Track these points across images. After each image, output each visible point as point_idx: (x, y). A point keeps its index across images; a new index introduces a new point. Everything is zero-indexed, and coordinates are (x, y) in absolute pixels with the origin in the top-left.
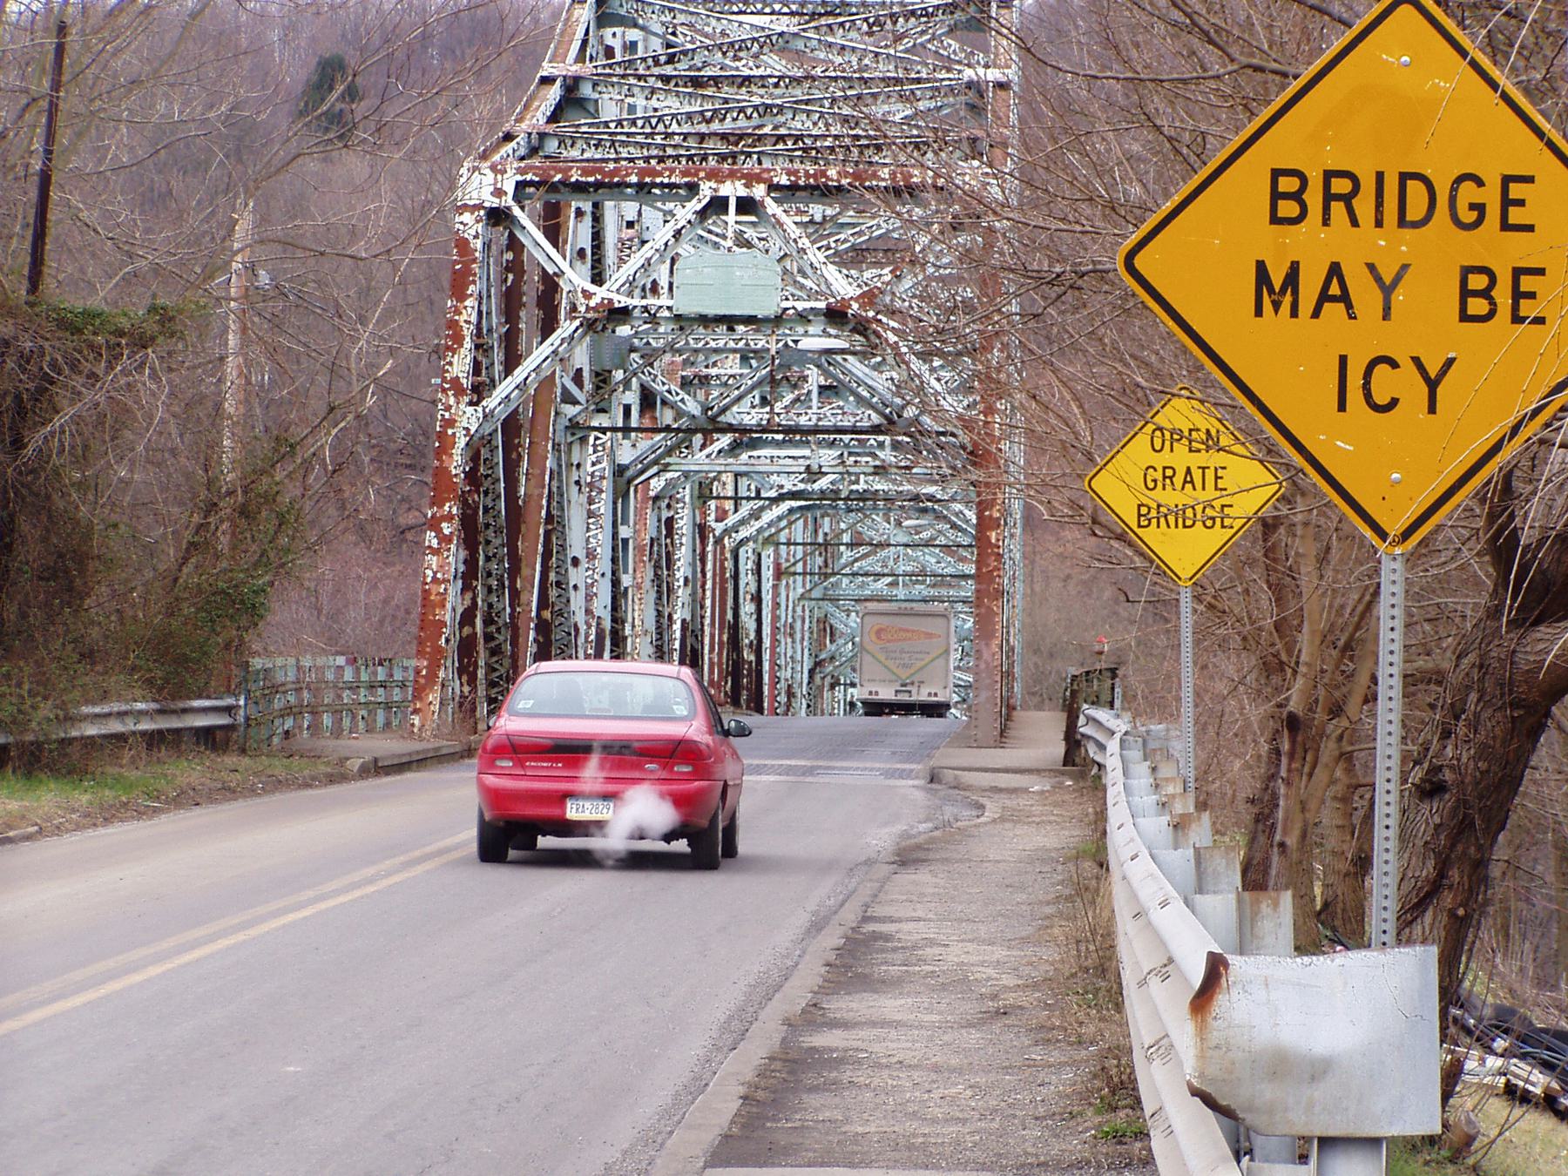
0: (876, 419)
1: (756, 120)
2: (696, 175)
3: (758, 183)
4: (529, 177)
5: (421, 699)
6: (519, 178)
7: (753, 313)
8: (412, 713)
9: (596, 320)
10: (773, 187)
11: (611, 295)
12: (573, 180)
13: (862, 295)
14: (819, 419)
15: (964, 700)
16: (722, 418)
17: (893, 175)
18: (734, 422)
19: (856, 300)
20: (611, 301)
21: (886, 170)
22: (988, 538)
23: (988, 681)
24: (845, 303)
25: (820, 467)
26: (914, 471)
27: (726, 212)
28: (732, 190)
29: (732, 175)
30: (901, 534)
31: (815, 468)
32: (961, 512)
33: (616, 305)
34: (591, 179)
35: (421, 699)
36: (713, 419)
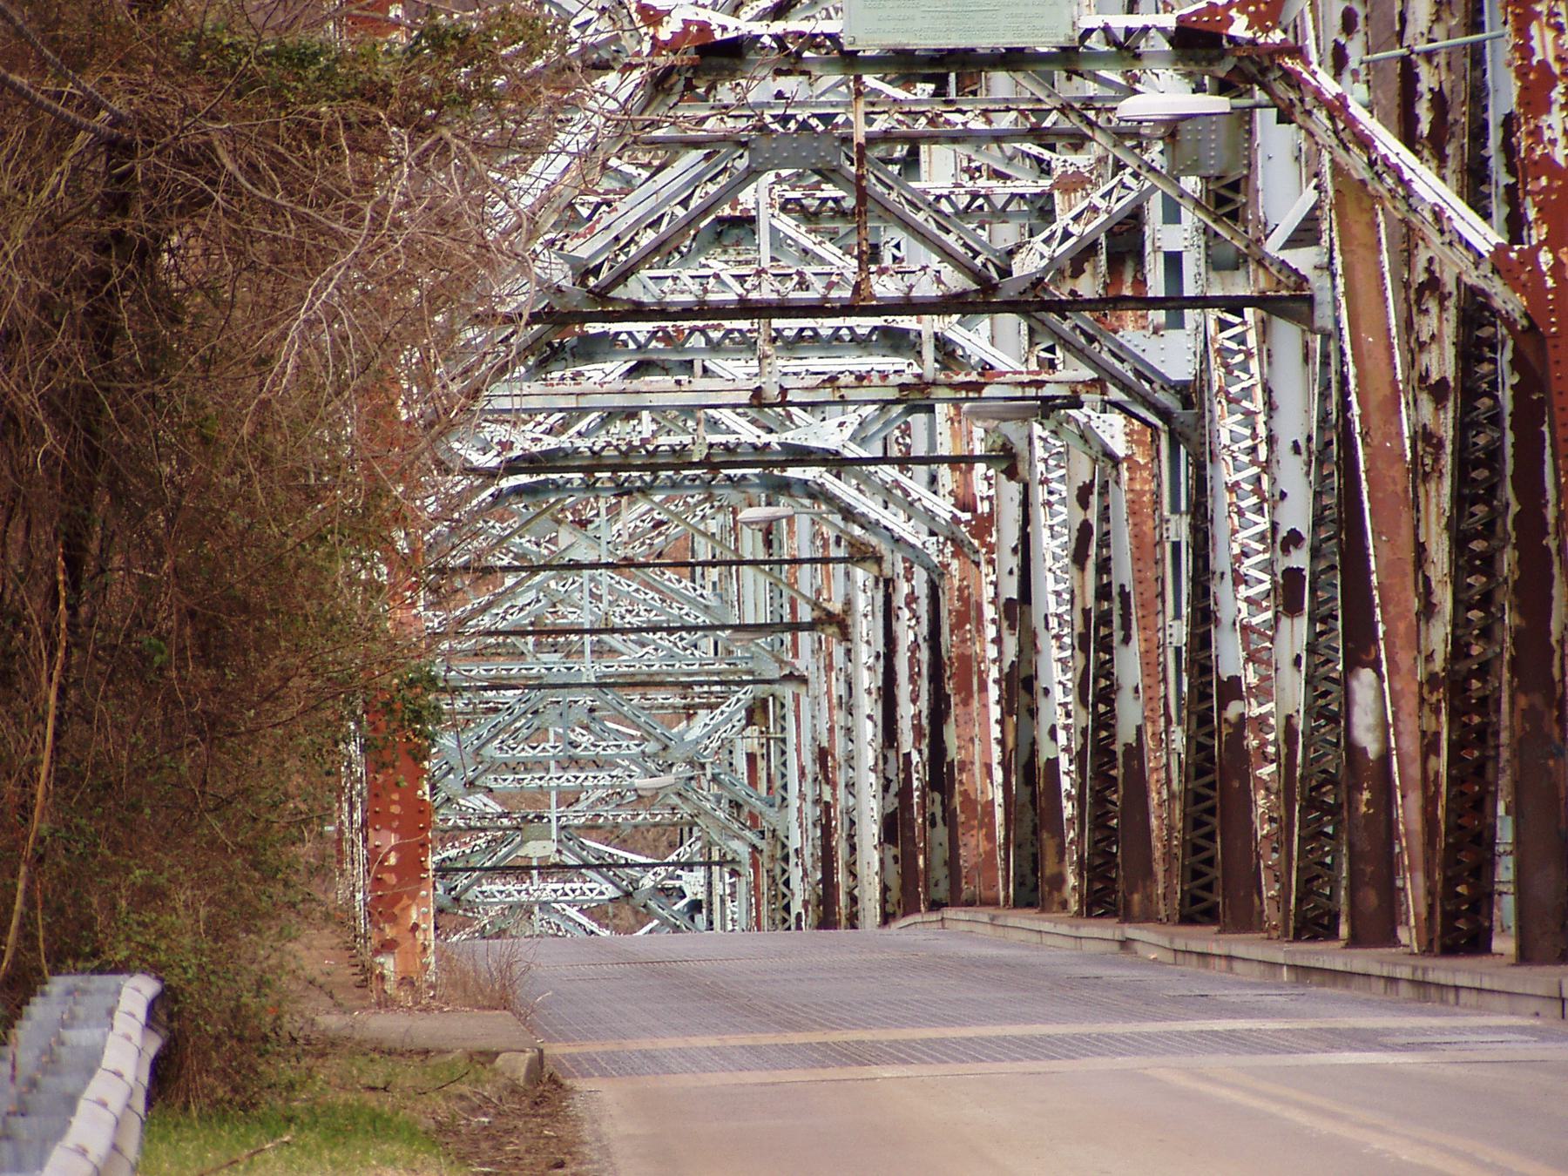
0: (956, 281)
5: (393, 919)
8: (377, 952)
11: (704, 15)
14: (830, 286)
15: (628, 895)
18: (645, 299)
20: (704, 27)
25: (784, 391)
26: (986, 392)
30: (584, 543)
31: (772, 393)
32: (897, 484)
33: (718, 36)
36: (601, 295)
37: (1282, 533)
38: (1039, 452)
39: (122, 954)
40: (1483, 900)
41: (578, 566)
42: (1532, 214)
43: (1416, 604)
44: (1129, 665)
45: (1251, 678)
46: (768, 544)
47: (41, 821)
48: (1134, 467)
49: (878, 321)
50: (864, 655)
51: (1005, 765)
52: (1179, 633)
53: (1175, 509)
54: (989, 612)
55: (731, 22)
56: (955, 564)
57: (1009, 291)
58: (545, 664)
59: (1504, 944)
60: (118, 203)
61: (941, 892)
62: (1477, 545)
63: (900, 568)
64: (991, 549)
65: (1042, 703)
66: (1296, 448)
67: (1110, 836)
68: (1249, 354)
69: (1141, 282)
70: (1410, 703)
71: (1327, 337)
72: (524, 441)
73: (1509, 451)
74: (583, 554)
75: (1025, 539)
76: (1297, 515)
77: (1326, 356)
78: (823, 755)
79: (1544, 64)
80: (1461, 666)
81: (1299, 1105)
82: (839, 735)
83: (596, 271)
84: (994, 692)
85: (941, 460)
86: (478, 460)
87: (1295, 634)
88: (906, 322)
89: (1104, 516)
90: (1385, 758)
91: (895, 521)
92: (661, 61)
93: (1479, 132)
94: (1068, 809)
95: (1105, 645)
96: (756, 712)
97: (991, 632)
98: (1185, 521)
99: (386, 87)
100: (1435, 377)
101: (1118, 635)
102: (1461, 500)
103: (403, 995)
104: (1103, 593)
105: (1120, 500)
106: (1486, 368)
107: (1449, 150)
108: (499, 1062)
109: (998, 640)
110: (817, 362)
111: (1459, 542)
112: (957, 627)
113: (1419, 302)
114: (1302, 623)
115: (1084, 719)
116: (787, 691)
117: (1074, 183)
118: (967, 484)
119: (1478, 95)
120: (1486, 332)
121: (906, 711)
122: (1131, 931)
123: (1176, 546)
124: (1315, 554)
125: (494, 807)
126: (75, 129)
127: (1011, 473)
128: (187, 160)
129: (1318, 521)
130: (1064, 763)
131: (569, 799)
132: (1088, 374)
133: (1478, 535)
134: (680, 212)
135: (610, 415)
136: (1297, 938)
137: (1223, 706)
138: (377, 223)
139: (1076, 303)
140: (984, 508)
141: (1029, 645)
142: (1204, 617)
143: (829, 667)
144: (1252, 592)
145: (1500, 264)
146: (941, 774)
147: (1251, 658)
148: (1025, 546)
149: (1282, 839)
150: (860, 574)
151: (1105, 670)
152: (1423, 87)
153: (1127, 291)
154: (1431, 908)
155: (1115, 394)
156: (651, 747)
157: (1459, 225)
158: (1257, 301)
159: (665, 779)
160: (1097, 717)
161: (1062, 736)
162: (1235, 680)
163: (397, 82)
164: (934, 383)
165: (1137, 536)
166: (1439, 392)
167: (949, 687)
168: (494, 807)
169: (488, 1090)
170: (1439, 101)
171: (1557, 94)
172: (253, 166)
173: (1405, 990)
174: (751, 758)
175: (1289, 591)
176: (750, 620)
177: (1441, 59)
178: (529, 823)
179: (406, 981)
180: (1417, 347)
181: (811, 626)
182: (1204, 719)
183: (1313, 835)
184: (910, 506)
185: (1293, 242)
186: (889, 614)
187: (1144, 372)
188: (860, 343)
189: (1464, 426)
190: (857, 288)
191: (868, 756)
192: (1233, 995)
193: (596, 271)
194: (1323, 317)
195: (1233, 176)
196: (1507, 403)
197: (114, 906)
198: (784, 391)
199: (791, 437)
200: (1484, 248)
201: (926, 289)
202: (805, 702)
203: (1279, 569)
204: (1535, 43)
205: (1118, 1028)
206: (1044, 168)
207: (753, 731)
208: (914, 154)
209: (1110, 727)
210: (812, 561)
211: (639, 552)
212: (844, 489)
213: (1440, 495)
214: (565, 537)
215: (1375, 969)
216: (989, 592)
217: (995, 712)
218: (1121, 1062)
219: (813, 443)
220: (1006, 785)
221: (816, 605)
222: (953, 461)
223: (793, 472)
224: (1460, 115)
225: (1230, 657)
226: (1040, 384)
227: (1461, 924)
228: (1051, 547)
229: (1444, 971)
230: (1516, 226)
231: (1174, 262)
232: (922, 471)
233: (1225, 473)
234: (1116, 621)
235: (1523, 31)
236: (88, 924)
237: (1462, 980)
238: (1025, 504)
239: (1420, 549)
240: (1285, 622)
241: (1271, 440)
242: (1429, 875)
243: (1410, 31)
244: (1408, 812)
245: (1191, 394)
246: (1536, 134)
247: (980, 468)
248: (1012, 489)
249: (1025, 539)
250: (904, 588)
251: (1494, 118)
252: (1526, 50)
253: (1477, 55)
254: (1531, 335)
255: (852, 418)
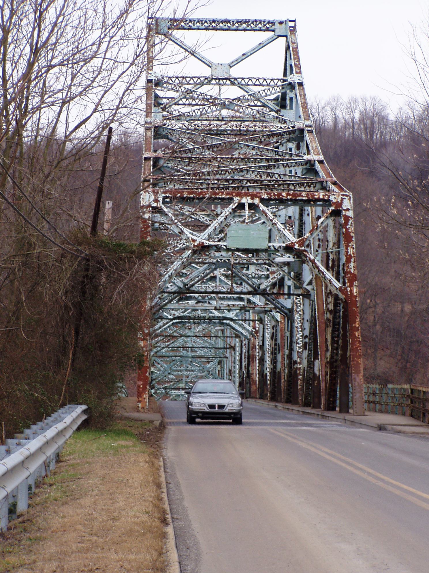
0: (250, 289)
1: (232, 174)
2: (232, 195)
3: (256, 198)
4: (168, 195)
5: (141, 397)
6: (164, 195)
7: (257, 248)
9: (197, 250)
10: (262, 200)
11: (203, 241)
12: (185, 196)
13: (300, 241)
16: (191, 289)
17: (307, 195)
19: (297, 243)
20: (203, 243)
21: (304, 193)
22: (355, 335)
23: (359, 390)
24: (293, 244)
25: (220, 307)
26: (256, 309)
27: (244, 209)
28: (247, 200)
29: (246, 195)
31: (218, 307)
33: (205, 244)
34: (192, 196)
35: (141, 397)
36: (188, 289)
37: (305, 335)
38: (266, 319)
39: (81, 401)
40: (334, 402)
41: (189, 336)
42: (347, 281)
43: (325, 349)
44: (279, 357)
45: (298, 361)
46: (223, 334)
47: (68, 377)
48: (281, 323)
49: (238, 296)
50: (237, 354)
51: (259, 374)
52: (287, 352)
53: (288, 330)
54: (257, 347)
55: (208, 242)
56: (252, 339)
57: (259, 291)
58: (184, 353)
59: (338, 409)
60: (87, 270)
61: (248, 396)
62: (336, 339)
63: (243, 339)
64: (258, 336)
65: (265, 363)
66: (307, 321)
67: (275, 387)
68: (301, 304)
69: (283, 291)
70: (324, 366)
71: (313, 301)
72: (177, 314)
73: (341, 323)
74: (190, 334)
75: (263, 335)
76: (307, 332)
77: (312, 305)
78: (230, 371)
79: (350, 255)
80: (332, 360)
81: (291, 436)
82: (233, 368)
83: (187, 285)
84: (257, 361)
85: (250, 320)
86: (170, 317)
87: (306, 353)
88: (243, 296)
89: (276, 331)
90: (319, 376)
91: (243, 332)
92: (195, 248)
93: (339, 266)
94: (269, 382)
95: (275, 354)
96: (220, 363)
97: (257, 351)
98: (289, 333)
99: (135, 251)
100: (330, 309)
101: (277, 352)
102: (333, 331)
103: (142, 410)
104: (275, 345)
105: (279, 329)
106: (338, 308)
107: (335, 269)
108: (154, 423)
109: (259, 352)
110: (226, 302)
111: (332, 338)
112: (252, 350)
113: (328, 296)
114: (307, 351)
115: (272, 367)
116: (225, 359)
117: (273, 273)
118: (255, 324)
119: (339, 259)
120: (338, 302)
121: (244, 364)
122: (277, 404)
123: (288, 337)
124: (309, 339)
125: (174, 378)
126: (78, 257)
127: (261, 323)
128: (99, 263)
129: (310, 334)
130: (268, 374)
131: (187, 377)
132: (273, 306)
133: (335, 337)
134: (202, 275)
135: (194, 310)
136: (304, 406)
137: (294, 365)
138: (131, 275)
139: (273, 293)
140: (257, 329)
141: (263, 353)
142: (291, 350)
143: (232, 356)
144: (299, 346)
145: (340, 289)
146: (249, 375)
147: (299, 357)
148: (263, 336)
149: (302, 389)
150: (237, 340)
151: (275, 358)
152: (330, 258)
153: (281, 292)
154: (326, 402)
155: (278, 310)
156: (201, 368)
157: (333, 282)
158: (302, 295)
159: (203, 374)
160: (274, 366)
161: (268, 369)
162: (296, 361)
163: (137, 251)
164: (247, 307)
165: (281, 335)
166: (331, 312)
167: (250, 360)
168: (174, 378)
169: (151, 428)
170: (333, 260)
171: (352, 260)
172: (110, 264)
173: (320, 417)
174: (219, 371)
175: (305, 346)
176: (219, 347)
177: (334, 253)
178: (180, 381)
179: (143, 408)
180: (327, 304)
181: (228, 348)
182: (291, 367)
183: (308, 388)
184: (244, 328)
185: (308, 284)
186: (242, 347)
187: (283, 306)
188: (235, 299)
189: (334, 318)
190: (231, 290)
191: (237, 371)
192: (293, 416)
193: (187, 285)
194: (312, 298)
195: (299, 272)
196: (341, 315)
197: (81, 393)
198: (220, 307)
199: (224, 315)
200: (338, 287)
201: (245, 290)
202: (228, 361)
203: (304, 342)
204: (349, 251)
205: (271, 421)
206: (268, 270)
207: (219, 366)
208: (248, 266)
209: (276, 368)
210: (230, 337)
211: (200, 334)
212: (232, 323)
213: (330, 330)
214: (187, 331)
215: (315, 412)
216: (258, 344)
217: (258, 365)
218: (264, 427)
219: (228, 316)
220: (259, 378)
221: (229, 345)
222: (253, 321)
223: (225, 321)
224: (336, 263)
225: (295, 357)
226: (265, 308)
227: (331, 405)
228: (268, 336)
229: (327, 413)
230: (344, 284)
231: (289, 287)
232: (247, 322)
233: (296, 325)
234: (277, 350)
235: (347, 249)
236: (76, 396)
237: (329, 415)
238: (264, 329)
239: (326, 339)
240: (304, 351)
241: (303, 319)
242: (325, 396)
243: (329, 248)
244: (323, 385)
245: (291, 310)
246: (348, 267)
247: (257, 322)
248: (262, 326)
249: (263, 335)
250: (244, 342)
251: (341, 264)
252: (347, 252)
253: (339, 253)
254: (346, 302)
255: (235, 312)
